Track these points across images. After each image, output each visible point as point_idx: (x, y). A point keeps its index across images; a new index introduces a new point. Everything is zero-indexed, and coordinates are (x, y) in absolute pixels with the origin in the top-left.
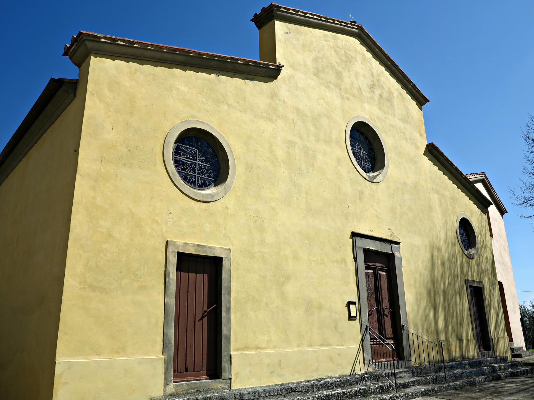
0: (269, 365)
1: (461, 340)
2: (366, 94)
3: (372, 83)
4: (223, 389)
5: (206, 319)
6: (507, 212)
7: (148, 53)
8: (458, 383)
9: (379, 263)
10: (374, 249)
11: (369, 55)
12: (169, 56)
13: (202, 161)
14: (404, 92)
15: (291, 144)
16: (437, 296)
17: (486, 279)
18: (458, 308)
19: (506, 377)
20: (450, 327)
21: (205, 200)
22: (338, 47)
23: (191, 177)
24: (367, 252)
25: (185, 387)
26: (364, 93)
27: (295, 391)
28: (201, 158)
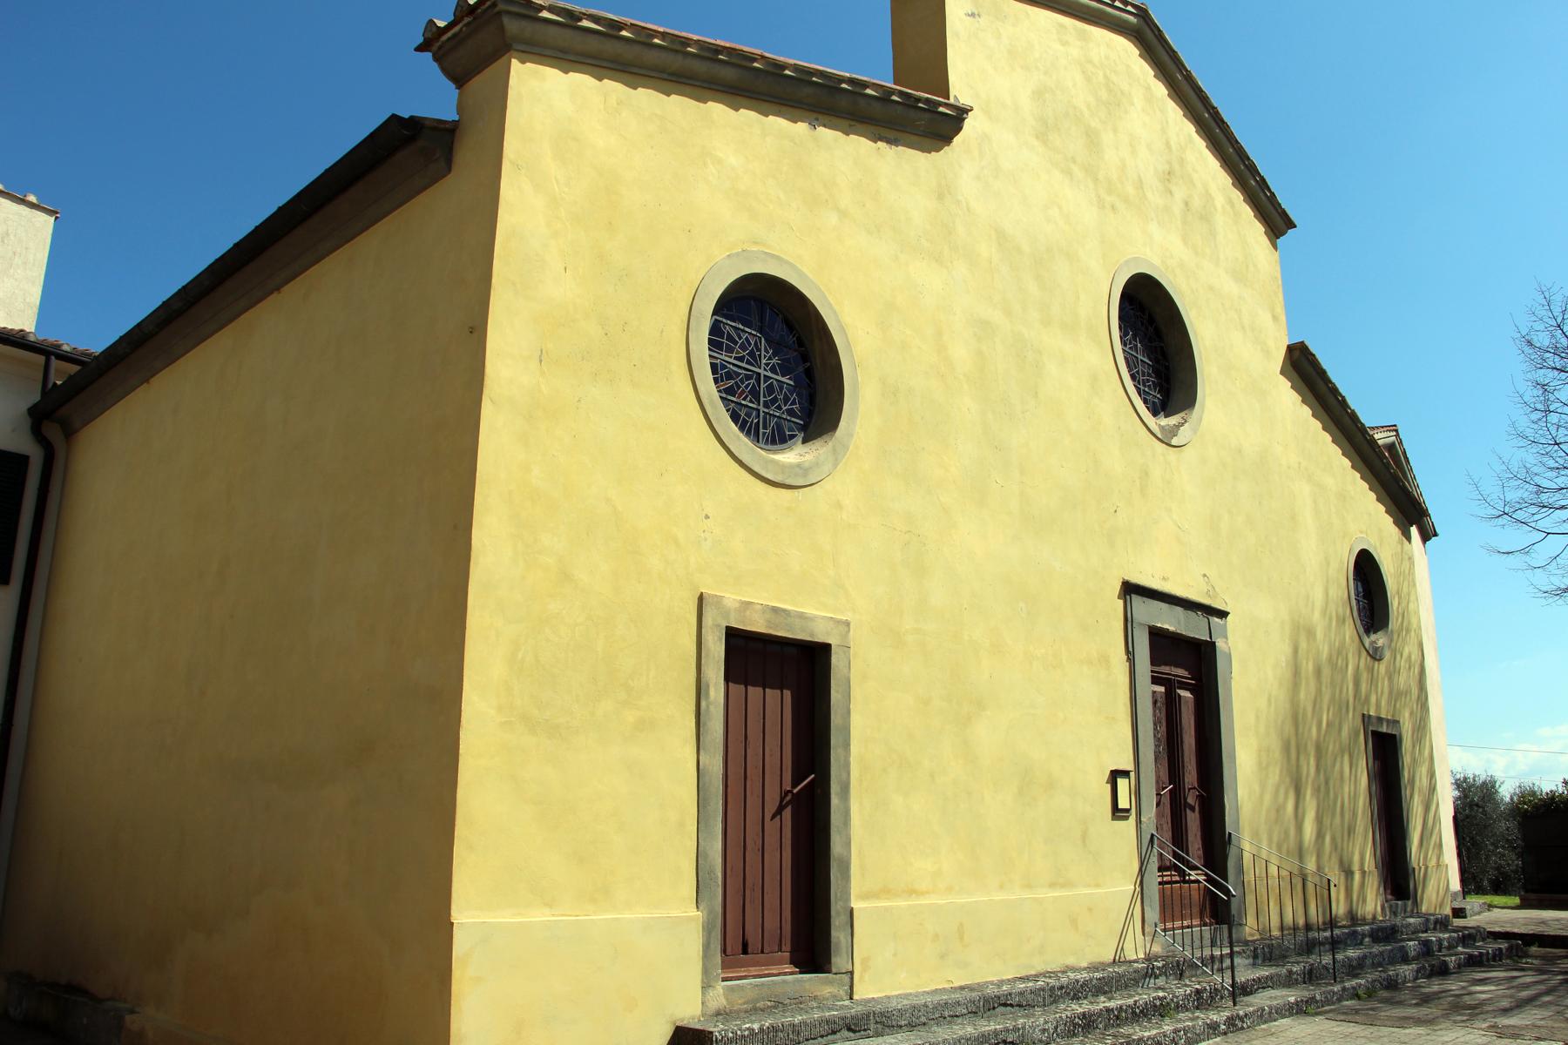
0: (936, 937)
1: (1349, 873)
3: (1167, 167)
4: (835, 997)
6: (1435, 535)
7: (651, 57)
9: (1181, 666)
10: (1172, 629)
11: (1160, 90)
13: (773, 370)
14: (1237, 196)
16: (1302, 758)
17: (1407, 715)
19: (1459, 966)
20: (1328, 839)
21: (788, 482)
22: (1090, 62)
24: (1156, 635)
26: (1149, 195)
27: (1005, 1005)
28: (777, 360)
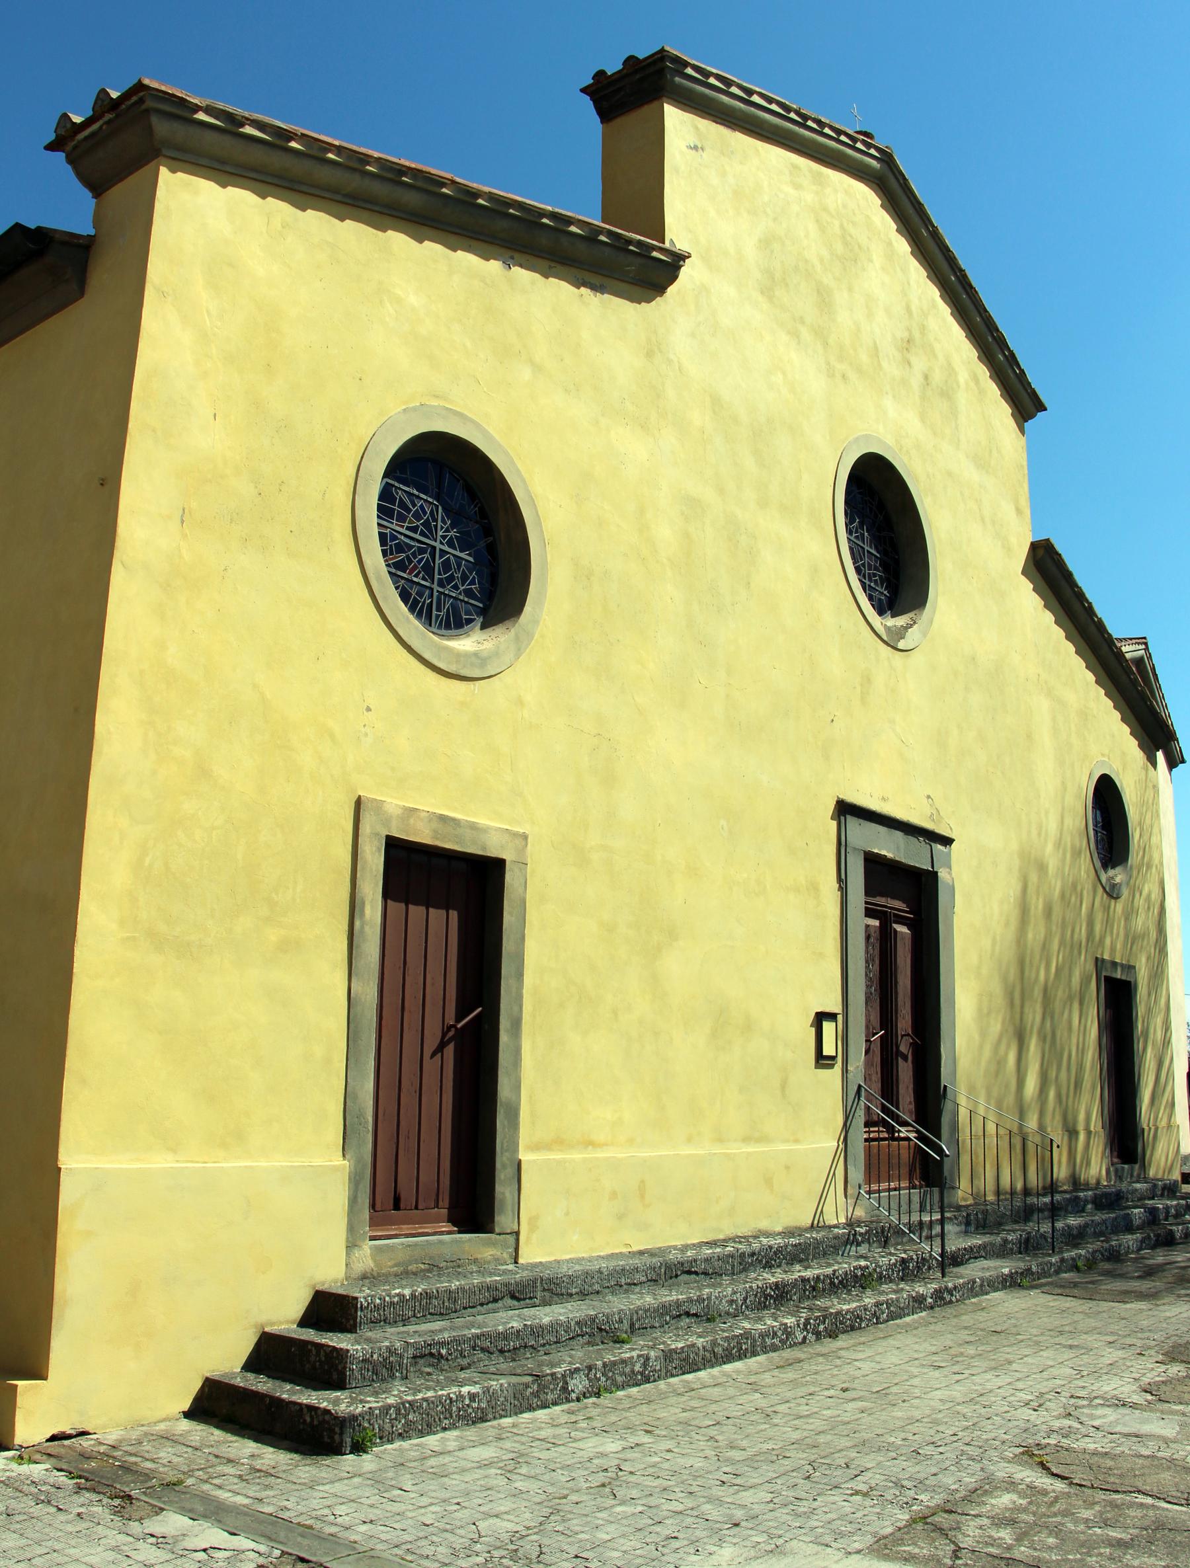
0: (614, 1195)
2: (891, 368)
3: (906, 335)
5: (450, 1050)
7: (324, 175)
8: (1083, 1252)
9: (899, 898)
10: (890, 855)
12: (381, 190)
13: (450, 544)
14: (983, 372)
15: (692, 507)
16: (1027, 1004)
17: (1144, 960)
18: (1074, 1041)
20: (1052, 1094)
21: (463, 672)
22: (825, 209)
23: (420, 594)
24: (873, 862)
25: (401, 1256)
26: (885, 364)
27: (689, 1272)
28: (455, 532)
